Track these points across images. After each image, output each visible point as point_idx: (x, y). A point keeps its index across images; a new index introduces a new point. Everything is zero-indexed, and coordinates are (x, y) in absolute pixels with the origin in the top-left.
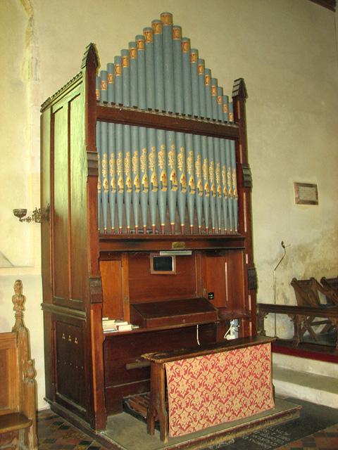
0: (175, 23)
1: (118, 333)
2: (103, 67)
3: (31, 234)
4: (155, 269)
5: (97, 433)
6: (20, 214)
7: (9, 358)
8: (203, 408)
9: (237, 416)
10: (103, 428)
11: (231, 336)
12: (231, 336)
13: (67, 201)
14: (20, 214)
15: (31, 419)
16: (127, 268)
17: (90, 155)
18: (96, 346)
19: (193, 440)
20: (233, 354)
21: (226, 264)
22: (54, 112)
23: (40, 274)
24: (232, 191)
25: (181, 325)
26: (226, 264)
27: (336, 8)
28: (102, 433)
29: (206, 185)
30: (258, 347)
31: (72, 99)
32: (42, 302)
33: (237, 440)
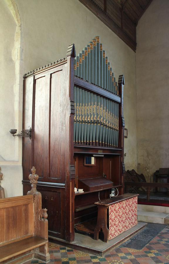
0: (100, 42)
1: (78, 193)
2: (77, 54)
3: (17, 143)
4: (86, 163)
5: (71, 243)
6: (13, 132)
7: (30, 209)
8: (115, 235)
9: (113, 236)
10: (73, 240)
11: (112, 195)
12: (112, 195)
13: (48, 129)
14: (13, 132)
15: (158, 181)
16: (78, 161)
17: (73, 105)
18: (72, 200)
19: (119, 241)
20: (112, 206)
21: (111, 161)
22: (35, 79)
23: (21, 165)
24: (117, 128)
25: (101, 190)
26: (111, 161)
27: (136, 51)
28: (73, 243)
29: (115, 127)
30: (113, 205)
31: (54, 73)
32: (22, 179)
33: (131, 239)
